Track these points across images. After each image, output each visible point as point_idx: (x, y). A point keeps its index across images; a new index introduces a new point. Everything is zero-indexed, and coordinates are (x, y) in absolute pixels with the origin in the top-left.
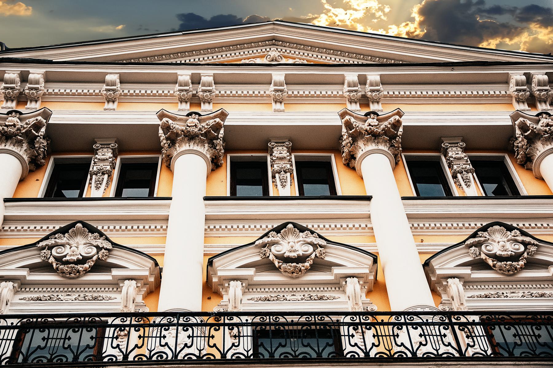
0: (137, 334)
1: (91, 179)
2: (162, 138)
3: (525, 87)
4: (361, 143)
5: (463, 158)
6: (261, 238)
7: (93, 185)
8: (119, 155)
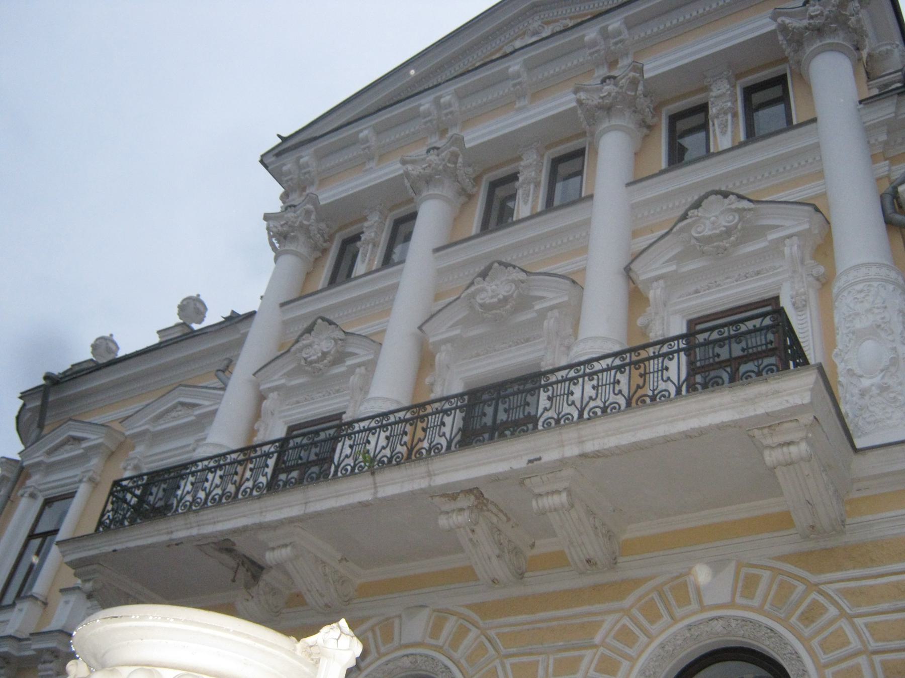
0: (638, 372)
1: (714, 125)
2: (784, 47)
6: (468, 288)
7: (718, 131)
8: (738, 82)
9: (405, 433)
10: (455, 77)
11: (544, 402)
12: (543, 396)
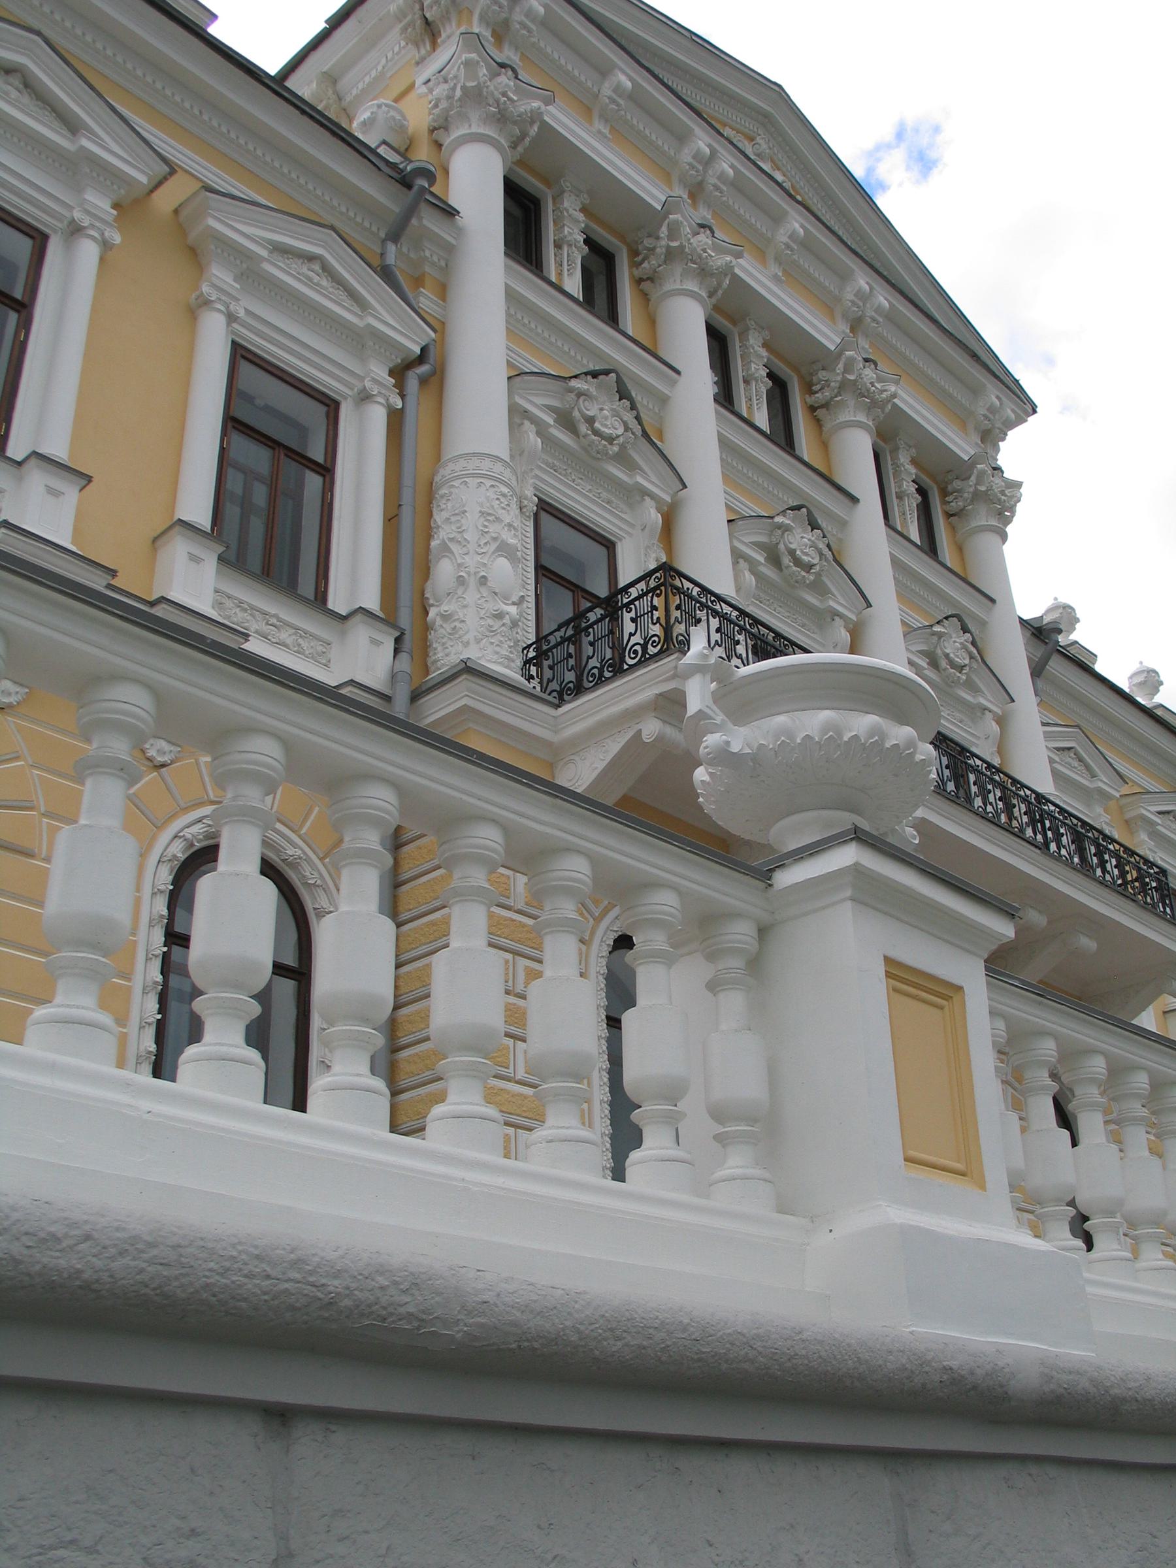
3: (621, 102)
4: (678, 269)
5: (579, 222)
9: (655, 608)
10: (171, 793)
11: (629, 627)
12: (627, 616)
